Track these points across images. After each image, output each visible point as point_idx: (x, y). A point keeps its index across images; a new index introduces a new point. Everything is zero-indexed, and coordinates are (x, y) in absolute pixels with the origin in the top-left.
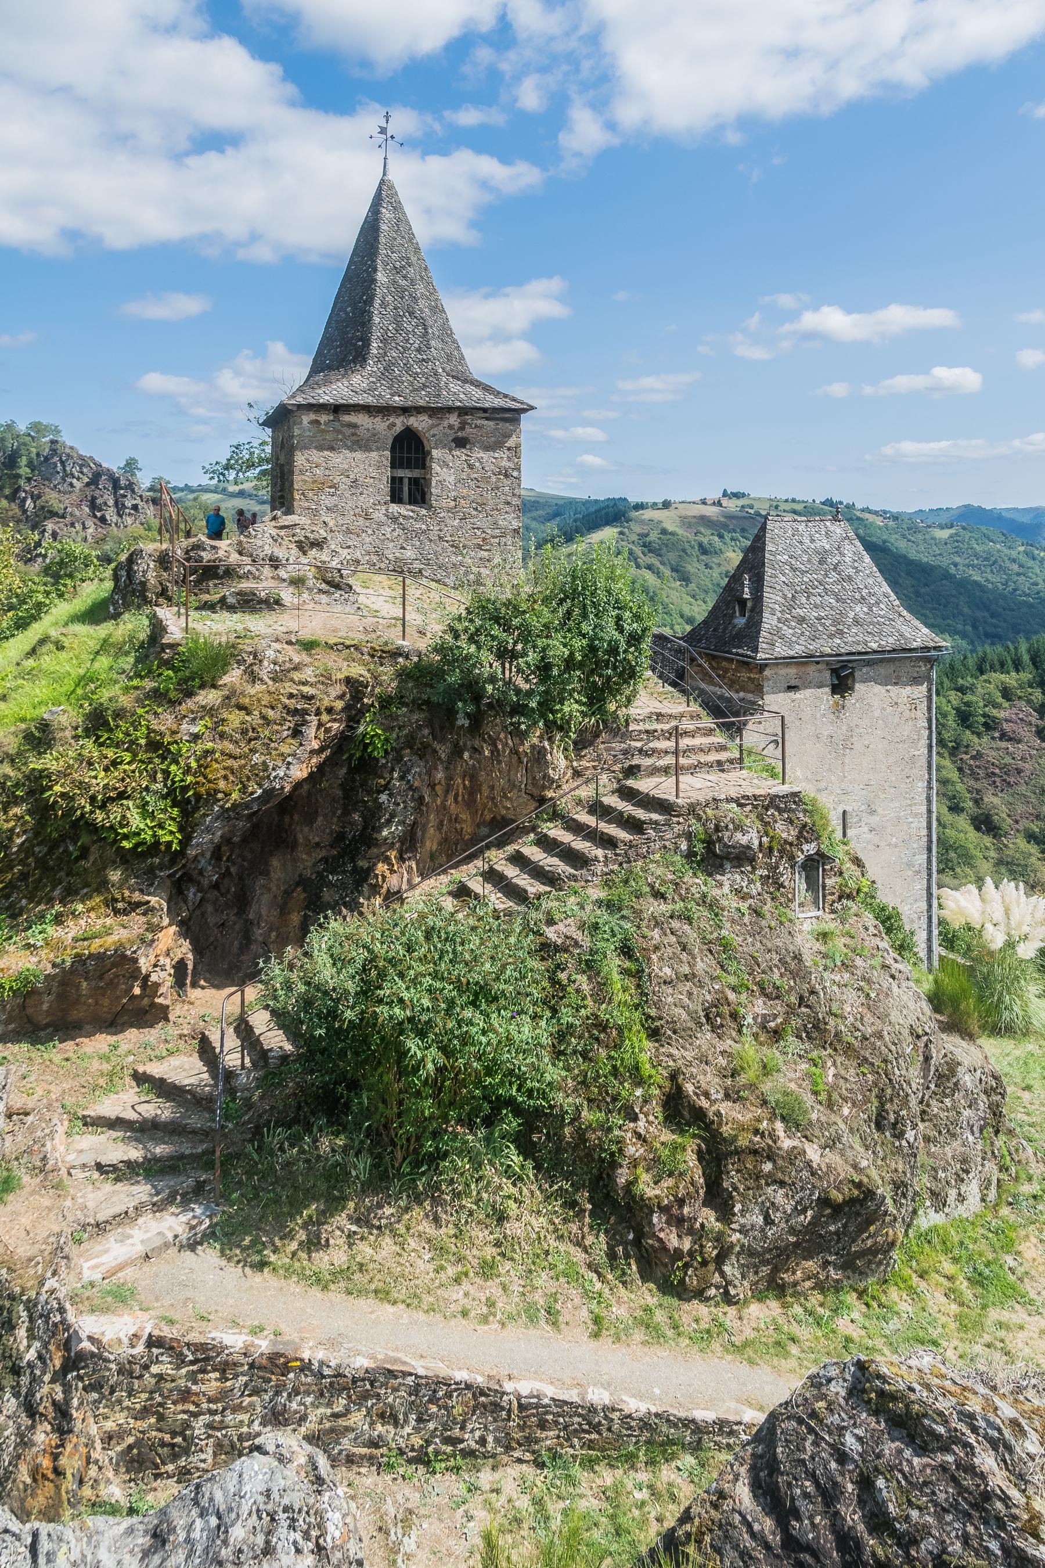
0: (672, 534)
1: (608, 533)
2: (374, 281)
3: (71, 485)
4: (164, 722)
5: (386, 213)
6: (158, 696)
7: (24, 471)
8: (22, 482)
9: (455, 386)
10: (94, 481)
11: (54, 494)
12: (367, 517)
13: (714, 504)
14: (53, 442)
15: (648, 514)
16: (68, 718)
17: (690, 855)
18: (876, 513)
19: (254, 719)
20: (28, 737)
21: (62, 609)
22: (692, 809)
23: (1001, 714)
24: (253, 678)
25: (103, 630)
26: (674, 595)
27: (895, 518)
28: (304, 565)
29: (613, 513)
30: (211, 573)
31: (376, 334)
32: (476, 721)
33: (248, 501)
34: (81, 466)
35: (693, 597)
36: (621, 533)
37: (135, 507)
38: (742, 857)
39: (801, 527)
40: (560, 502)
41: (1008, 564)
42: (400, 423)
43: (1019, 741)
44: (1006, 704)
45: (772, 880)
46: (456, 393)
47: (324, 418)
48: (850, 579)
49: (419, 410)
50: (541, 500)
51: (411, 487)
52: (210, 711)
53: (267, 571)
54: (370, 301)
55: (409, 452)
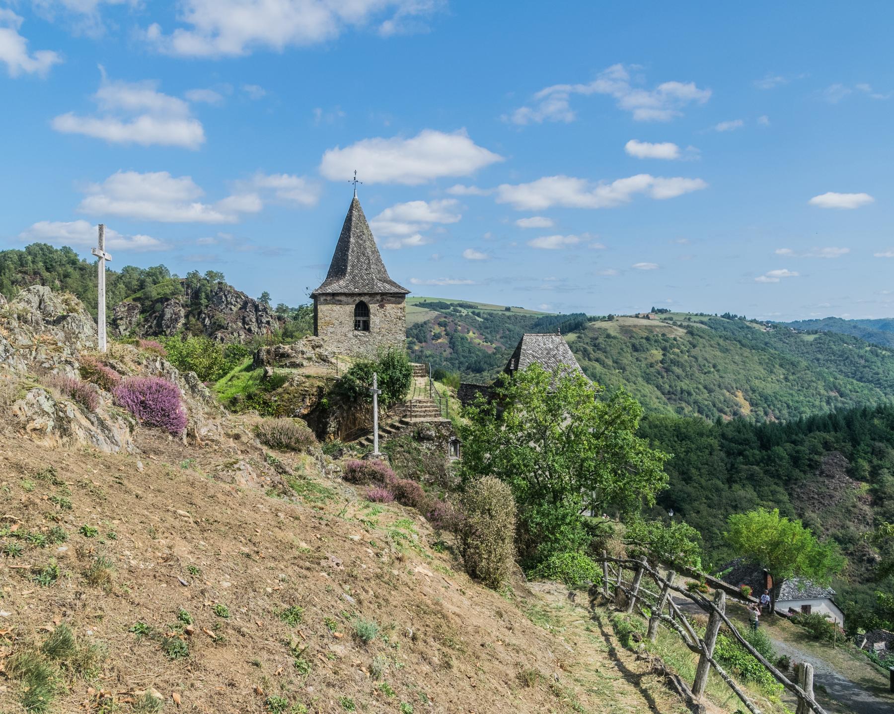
0: (614, 338)
2: (349, 242)
3: (231, 309)
4: (267, 396)
5: (355, 213)
6: (266, 390)
7: (204, 301)
8: (203, 308)
9: (379, 285)
10: (245, 304)
11: (221, 315)
12: (345, 335)
13: (643, 317)
14: (220, 283)
15: (598, 324)
16: (241, 396)
17: (414, 437)
18: (761, 323)
19: (291, 396)
20: (231, 401)
21: (237, 369)
22: (415, 424)
23: (822, 459)
24: (292, 385)
25: (250, 374)
27: (775, 326)
28: (310, 353)
30: (284, 356)
31: (350, 264)
32: (355, 398)
34: (237, 297)
35: (627, 380)
36: (579, 337)
37: (268, 323)
38: (429, 438)
39: (540, 338)
40: (540, 317)
41: (857, 359)
42: (358, 300)
43: (833, 477)
44: (826, 453)
45: (440, 446)
46: (381, 287)
47: (329, 298)
48: (560, 361)
49: (365, 294)
50: (528, 315)
52: (280, 394)
53: (300, 355)
54: (347, 250)
55: (362, 310)
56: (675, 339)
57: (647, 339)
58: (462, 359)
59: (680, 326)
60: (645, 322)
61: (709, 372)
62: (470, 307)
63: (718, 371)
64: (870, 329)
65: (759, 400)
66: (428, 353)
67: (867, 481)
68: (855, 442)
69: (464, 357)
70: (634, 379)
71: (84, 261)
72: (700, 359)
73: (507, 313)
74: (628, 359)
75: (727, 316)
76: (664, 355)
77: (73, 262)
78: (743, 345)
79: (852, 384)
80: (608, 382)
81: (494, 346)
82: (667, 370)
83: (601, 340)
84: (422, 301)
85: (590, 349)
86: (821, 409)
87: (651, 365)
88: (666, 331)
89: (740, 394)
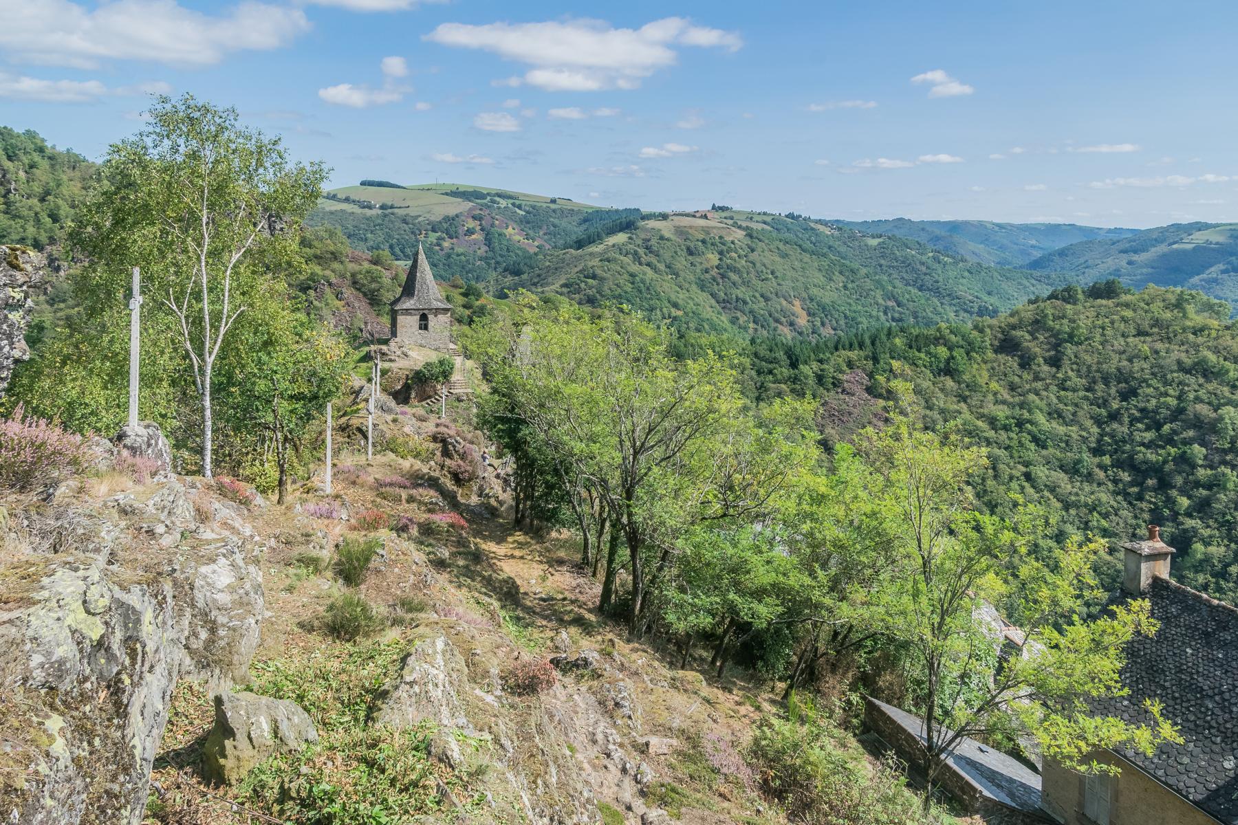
0: (668, 240)
1: (621, 238)
13: (701, 217)
15: (651, 224)
23: (845, 377)
26: (666, 286)
28: (399, 353)
29: (627, 222)
33: (352, 205)
35: (680, 287)
44: (848, 371)
51: (424, 326)
55: (424, 318)
56: (733, 242)
57: (704, 242)
58: (499, 259)
59: (740, 227)
60: (702, 222)
61: (766, 279)
62: (510, 197)
63: (776, 277)
64: (937, 232)
65: (817, 310)
66: (460, 250)
67: (884, 399)
68: (875, 360)
69: (502, 256)
70: (687, 285)
71: (53, 147)
72: (758, 265)
73: (553, 206)
74: (681, 263)
75: (791, 216)
76: (720, 259)
77: (41, 150)
78: (804, 250)
79: (909, 293)
80: (659, 290)
81: (536, 243)
82: (723, 276)
83: (653, 242)
84: (454, 189)
85: (641, 251)
86: (878, 319)
87: (707, 272)
88: (723, 233)
89: (797, 303)
